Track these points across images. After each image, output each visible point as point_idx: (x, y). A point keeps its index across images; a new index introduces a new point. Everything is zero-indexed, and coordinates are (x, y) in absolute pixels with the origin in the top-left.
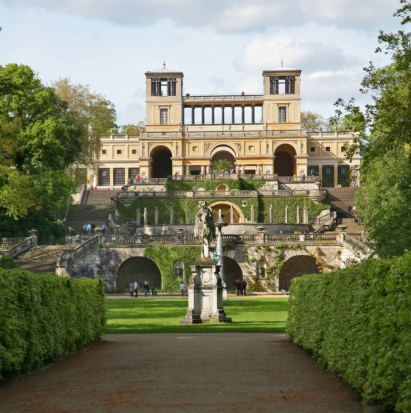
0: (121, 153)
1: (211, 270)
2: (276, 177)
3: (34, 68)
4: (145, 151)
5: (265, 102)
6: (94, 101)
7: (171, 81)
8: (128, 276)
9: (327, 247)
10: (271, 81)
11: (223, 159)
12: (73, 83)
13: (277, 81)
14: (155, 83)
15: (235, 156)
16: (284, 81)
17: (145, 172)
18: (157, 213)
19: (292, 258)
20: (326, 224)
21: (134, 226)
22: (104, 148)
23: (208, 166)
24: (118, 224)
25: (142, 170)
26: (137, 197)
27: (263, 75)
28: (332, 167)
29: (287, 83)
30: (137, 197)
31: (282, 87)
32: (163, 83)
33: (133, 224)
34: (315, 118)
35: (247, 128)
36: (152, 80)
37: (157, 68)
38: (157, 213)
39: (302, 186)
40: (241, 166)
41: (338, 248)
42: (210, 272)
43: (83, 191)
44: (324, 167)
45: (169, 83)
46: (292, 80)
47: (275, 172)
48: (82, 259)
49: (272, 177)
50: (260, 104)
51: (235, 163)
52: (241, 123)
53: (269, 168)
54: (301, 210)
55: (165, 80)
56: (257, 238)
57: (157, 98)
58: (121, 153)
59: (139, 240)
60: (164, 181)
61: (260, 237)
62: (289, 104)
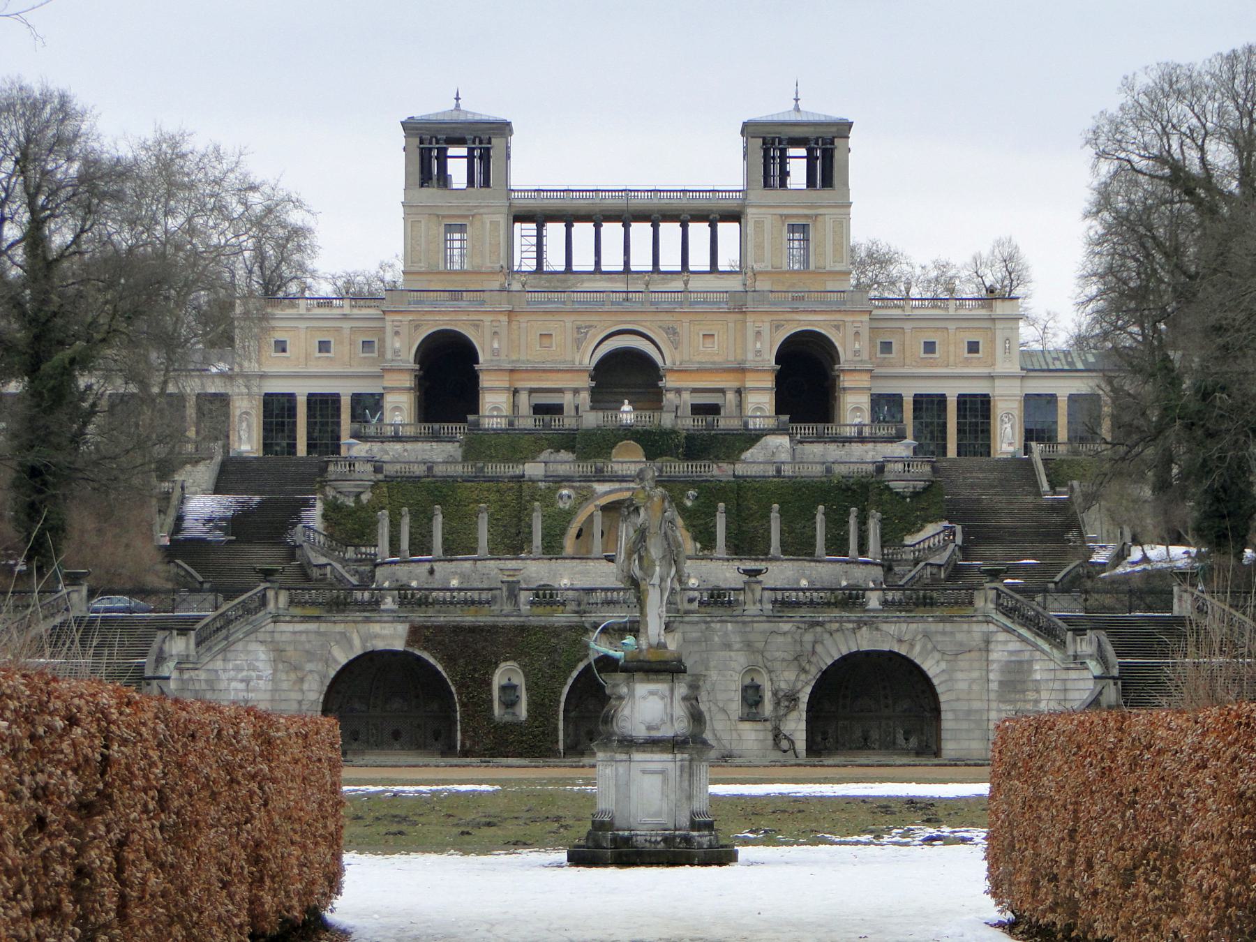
0: (320, 351)
1: (672, 691)
2: (784, 423)
3: (79, 101)
4: (403, 348)
5: (749, 211)
6: (254, 198)
7: (477, 144)
8: (357, 706)
9: (948, 627)
10: (766, 151)
11: (626, 373)
12: (196, 145)
13: (783, 151)
14: (430, 150)
15: (660, 363)
16: (802, 152)
17: (400, 408)
18: (438, 522)
19: (844, 659)
20: (931, 561)
21: (372, 560)
22: (280, 336)
23: (583, 389)
24: (324, 555)
25: (390, 400)
26: (380, 477)
27: (743, 133)
28: (941, 400)
29: (811, 159)
30: (380, 477)
31: (797, 170)
32: (452, 151)
33: (366, 554)
34: (889, 261)
35: (695, 284)
36: (421, 142)
37: (433, 105)
38: (438, 522)
39: (857, 450)
40: (678, 391)
41: (978, 629)
42: (667, 693)
43: (218, 458)
44: (919, 400)
45: (471, 151)
46: (824, 151)
47: (779, 410)
48: (220, 657)
49: (771, 423)
50: (734, 216)
51: (661, 384)
52: (679, 269)
53: (760, 403)
54: (862, 522)
55: (459, 142)
56: (741, 598)
57: (431, 194)
58: (320, 351)
59: (389, 600)
60: (458, 430)
61: (749, 595)
62: (816, 216)
